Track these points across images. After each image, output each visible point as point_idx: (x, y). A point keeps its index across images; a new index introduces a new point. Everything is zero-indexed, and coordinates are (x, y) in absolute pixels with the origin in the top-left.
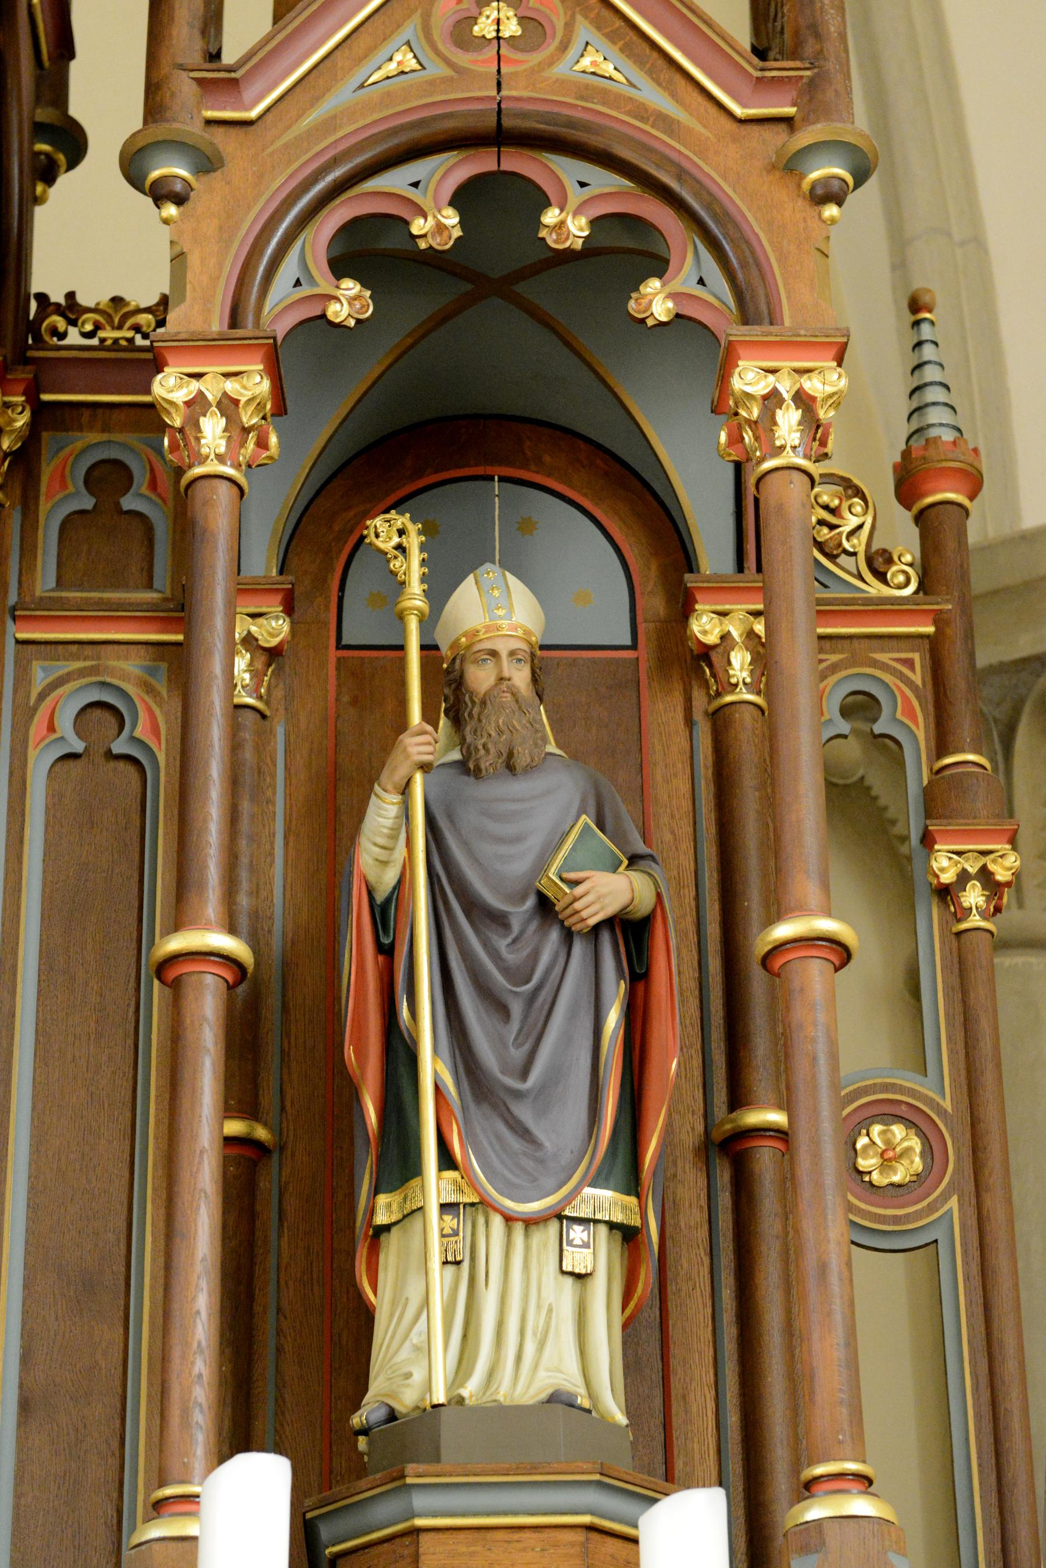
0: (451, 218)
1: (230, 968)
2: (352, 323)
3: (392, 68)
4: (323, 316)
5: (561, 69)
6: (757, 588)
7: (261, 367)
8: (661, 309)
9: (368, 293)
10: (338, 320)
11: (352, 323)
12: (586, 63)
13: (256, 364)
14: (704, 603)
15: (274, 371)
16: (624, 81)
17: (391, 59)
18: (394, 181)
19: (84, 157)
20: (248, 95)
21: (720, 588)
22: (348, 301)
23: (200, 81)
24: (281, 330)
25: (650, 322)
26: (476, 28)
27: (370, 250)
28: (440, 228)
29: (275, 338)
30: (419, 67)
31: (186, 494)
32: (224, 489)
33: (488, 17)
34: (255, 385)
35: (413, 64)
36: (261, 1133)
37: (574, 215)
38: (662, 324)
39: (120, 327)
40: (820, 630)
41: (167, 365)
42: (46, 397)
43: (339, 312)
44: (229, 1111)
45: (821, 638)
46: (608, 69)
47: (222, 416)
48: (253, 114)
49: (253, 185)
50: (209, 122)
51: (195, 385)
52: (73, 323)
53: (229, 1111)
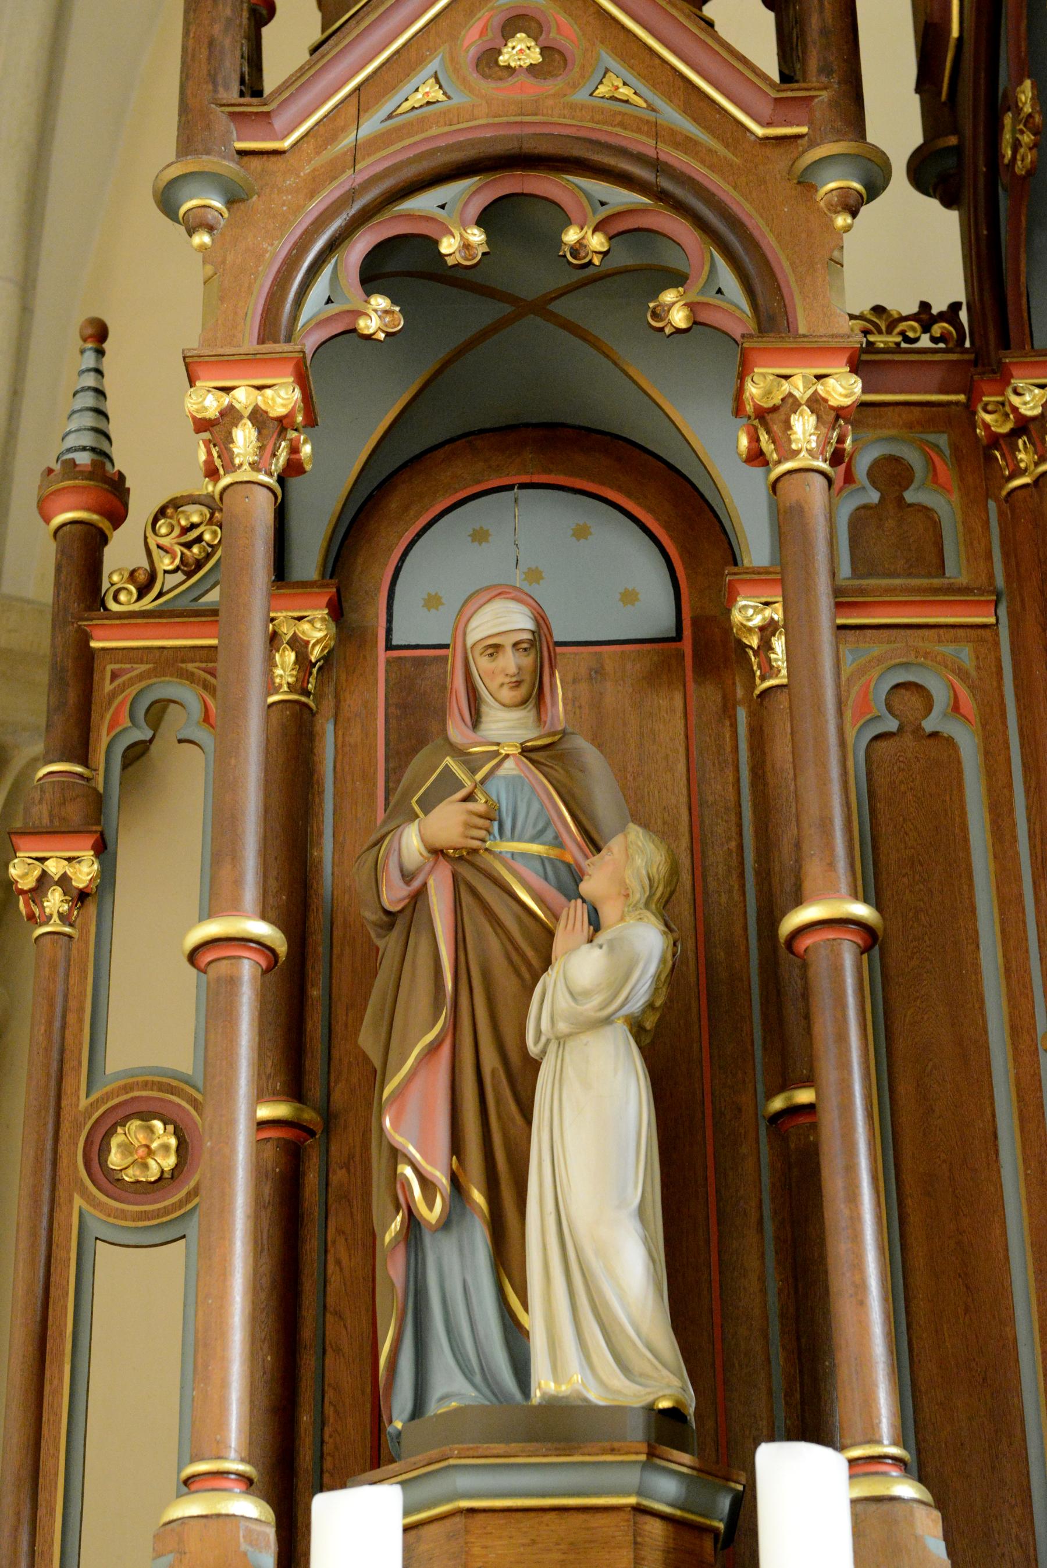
0: (477, 236)
1: (267, 956)
2: (381, 336)
3: (417, 99)
4: (354, 330)
5: (581, 96)
6: (773, 580)
7: (291, 379)
8: (679, 318)
9: (397, 309)
10: (366, 332)
11: (381, 336)
12: (602, 90)
13: (842, 367)
14: (746, 598)
15: (302, 380)
16: (644, 105)
17: (417, 90)
18: (424, 202)
19: (911, 183)
20: (279, 123)
21: (760, 578)
22: (378, 315)
23: (232, 115)
24: (310, 344)
25: (668, 330)
26: (501, 58)
27: (400, 265)
28: (467, 246)
29: (304, 352)
30: (445, 98)
31: (221, 499)
32: (819, 481)
33: (513, 48)
34: (283, 398)
35: (440, 96)
36: (309, 1116)
37: (594, 232)
38: (679, 331)
39: (889, 331)
40: (840, 621)
41: (199, 379)
42: (962, 397)
43: (369, 326)
44: (261, 1096)
45: (841, 627)
46: (625, 92)
47: (812, 412)
48: (287, 144)
49: (295, 211)
50: (242, 153)
51: (226, 400)
52: (926, 329)
53: (261, 1096)
